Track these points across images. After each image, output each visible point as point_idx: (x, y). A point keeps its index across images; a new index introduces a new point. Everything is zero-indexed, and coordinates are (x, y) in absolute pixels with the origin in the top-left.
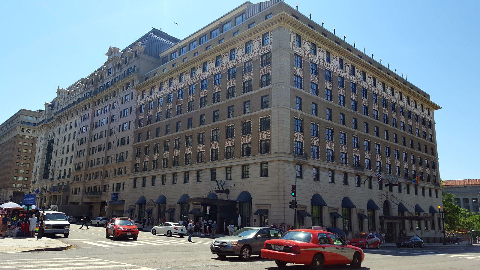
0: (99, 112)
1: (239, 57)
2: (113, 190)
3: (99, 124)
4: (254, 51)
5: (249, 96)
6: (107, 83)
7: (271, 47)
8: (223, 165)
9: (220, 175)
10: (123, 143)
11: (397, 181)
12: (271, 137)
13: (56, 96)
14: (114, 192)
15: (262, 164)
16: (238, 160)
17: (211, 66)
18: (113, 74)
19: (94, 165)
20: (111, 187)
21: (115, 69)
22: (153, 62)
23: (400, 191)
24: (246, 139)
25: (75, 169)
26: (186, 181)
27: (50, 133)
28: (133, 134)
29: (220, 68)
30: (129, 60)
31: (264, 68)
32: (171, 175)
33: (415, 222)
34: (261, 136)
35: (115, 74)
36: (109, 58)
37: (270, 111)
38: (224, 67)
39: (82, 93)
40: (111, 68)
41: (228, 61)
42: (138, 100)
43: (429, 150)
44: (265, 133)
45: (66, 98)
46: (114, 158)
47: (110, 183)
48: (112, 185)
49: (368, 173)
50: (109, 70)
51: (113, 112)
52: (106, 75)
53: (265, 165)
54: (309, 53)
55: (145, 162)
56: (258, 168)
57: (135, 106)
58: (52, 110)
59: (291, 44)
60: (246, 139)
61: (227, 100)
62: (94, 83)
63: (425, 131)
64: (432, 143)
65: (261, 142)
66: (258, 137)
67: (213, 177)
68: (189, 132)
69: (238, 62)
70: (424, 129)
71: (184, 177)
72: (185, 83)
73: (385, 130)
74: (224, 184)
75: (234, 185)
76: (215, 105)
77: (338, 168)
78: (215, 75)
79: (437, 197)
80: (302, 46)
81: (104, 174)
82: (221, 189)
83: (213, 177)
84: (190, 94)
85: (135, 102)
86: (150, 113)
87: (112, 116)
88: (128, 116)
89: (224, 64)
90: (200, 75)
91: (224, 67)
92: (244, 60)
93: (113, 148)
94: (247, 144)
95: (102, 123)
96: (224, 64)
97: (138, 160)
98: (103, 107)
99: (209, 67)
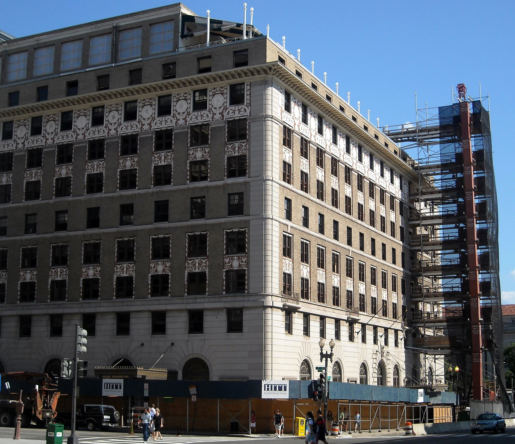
5: (202, 189)
7: (248, 111)
12: (248, 265)
17: (114, 117)
31: (92, 162)
38: (218, 115)
41: (153, 116)
44: (236, 258)
56: (223, 317)
61: (153, 189)
75: (173, 344)
78: (191, 126)
91: (218, 115)
96: (144, 119)
99: (110, 118)
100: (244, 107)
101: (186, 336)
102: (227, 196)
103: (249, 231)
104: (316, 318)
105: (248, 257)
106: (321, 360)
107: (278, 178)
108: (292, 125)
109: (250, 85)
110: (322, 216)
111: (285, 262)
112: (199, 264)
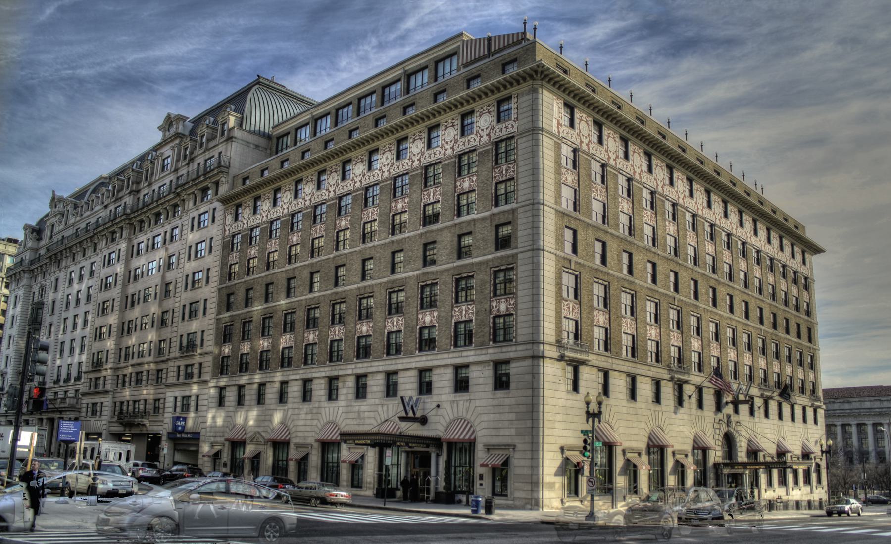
0: (143, 246)
1: (447, 143)
2: (175, 411)
3: (143, 272)
4: (481, 132)
6: (160, 187)
7: (516, 126)
8: (413, 365)
9: (408, 386)
10: (193, 314)
11: (747, 395)
12: (516, 308)
13: (48, 209)
14: (177, 414)
15: (497, 364)
16: (446, 356)
17: (387, 158)
18: (173, 169)
19: (133, 358)
20: (170, 404)
21: (178, 161)
22: (257, 146)
23: (752, 412)
24: (464, 312)
25: (92, 365)
26: (332, 394)
27: (36, 289)
28: (214, 295)
29: (405, 164)
30: (208, 140)
32: (300, 383)
33: (775, 473)
34: (496, 307)
35: (176, 170)
36: (164, 135)
37: (515, 256)
39: (106, 207)
40: (169, 156)
42: (227, 223)
43: (804, 332)
44: (503, 300)
45: (70, 216)
46: (176, 344)
47: (168, 394)
48: (172, 399)
49: (696, 378)
50: (164, 160)
51: (173, 248)
52: (157, 172)
53: (504, 367)
54: (589, 141)
55: (389, 333)
56: (488, 372)
57: (220, 237)
58: (39, 239)
59: (555, 123)
60: (464, 312)
62: (132, 186)
63: (797, 296)
64: (809, 319)
65: (494, 318)
66: (488, 309)
67: (391, 390)
68: (337, 293)
69: (445, 152)
70: (795, 292)
71: (327, 387)
72: (330, 192)
73: (728, 294)
74: (416, 403)
75: (438, 406)
76: (395, 238)
77: (616, 364)
79: (816, 422)
80: (576, 126)
81: (155, 377)
82: (411, 414)
83: (391, 390)
84: (339, 214)
85: (221, 227)
86: (253, 252)
87: (170, 257)
88: (204, 257)
89: (414, 155)
90: (363, 176)
92: (459, 150)
93: (172, 323)
94: (466, 322)
95: (148, 270)
96: (414, 155)
97: (227, 350)
98: (150, 235)
100: (511, 122)
101: (452, 397)
102: (494, 229)
103: (517, 267)
104: (620, 376)
105: (516, 298)
106: (587, 421)
107: (553, 201)
108: (730, 230)
109: (517, 97)
110: (799, 325)
111: (567, 305)
112: (466, 311)
